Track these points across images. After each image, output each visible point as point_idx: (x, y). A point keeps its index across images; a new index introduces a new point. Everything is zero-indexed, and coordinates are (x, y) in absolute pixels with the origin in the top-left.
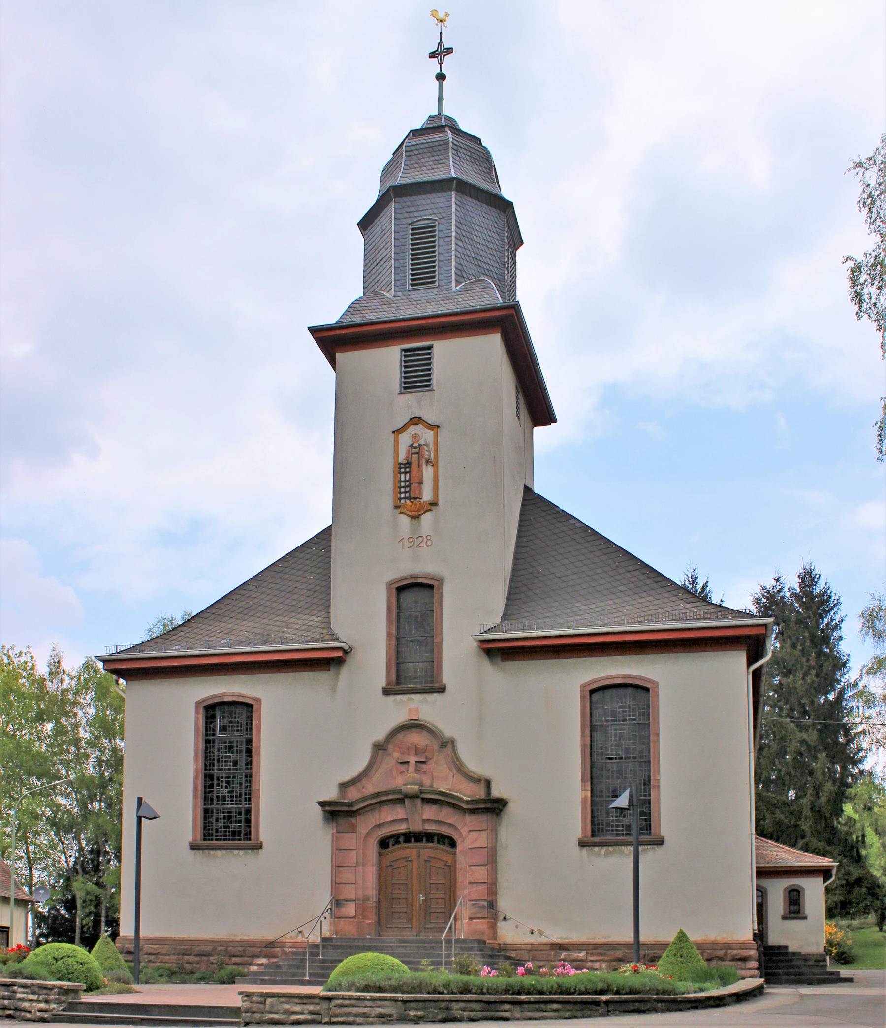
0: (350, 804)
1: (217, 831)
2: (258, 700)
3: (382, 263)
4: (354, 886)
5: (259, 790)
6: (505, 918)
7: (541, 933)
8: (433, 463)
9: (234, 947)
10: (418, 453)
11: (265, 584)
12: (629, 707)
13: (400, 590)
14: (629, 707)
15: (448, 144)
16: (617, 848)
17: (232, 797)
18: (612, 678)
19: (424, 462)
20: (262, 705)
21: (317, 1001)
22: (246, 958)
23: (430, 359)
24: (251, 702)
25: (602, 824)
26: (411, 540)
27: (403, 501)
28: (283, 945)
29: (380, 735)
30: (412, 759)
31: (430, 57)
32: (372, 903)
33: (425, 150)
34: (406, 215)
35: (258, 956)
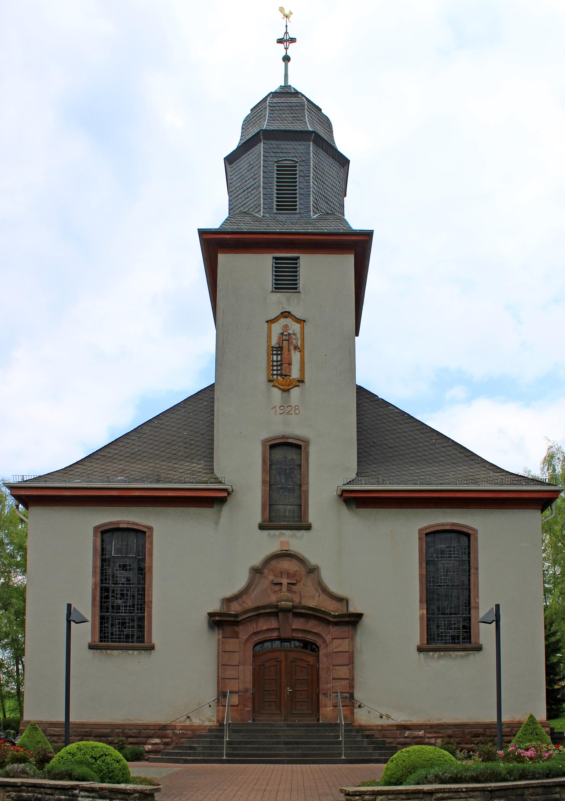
0: (236, 616)
1: (112, 634)
2: (151, 529)
3: (250, 190)
4: (237, 681)
5: (151, 602)
6: (360, 706)
7: (388, 717)
8: (300, 349)
9: (130, 730)
10: (288, 340)
11: (145, 436)
12: (454, 547)
13: (272, 447)
14: (454, 547)
15: (303, 106)
17: (126, 606)
18: (443, 525)
19: (292, 347)
20: (154, 533)
21: (421, 796)
22: (141, 739)
23: (296, 268)
24: (145, 530)
25: (434, 635)
26: (282, 408)
27: (275, 377)
28: (174, 728)
29: (257, 560)
30: (285, 581)
31: (278, 42)
32: (249, 694)
33: (286, 108)
34: (273, 155)
35: (151, 737)
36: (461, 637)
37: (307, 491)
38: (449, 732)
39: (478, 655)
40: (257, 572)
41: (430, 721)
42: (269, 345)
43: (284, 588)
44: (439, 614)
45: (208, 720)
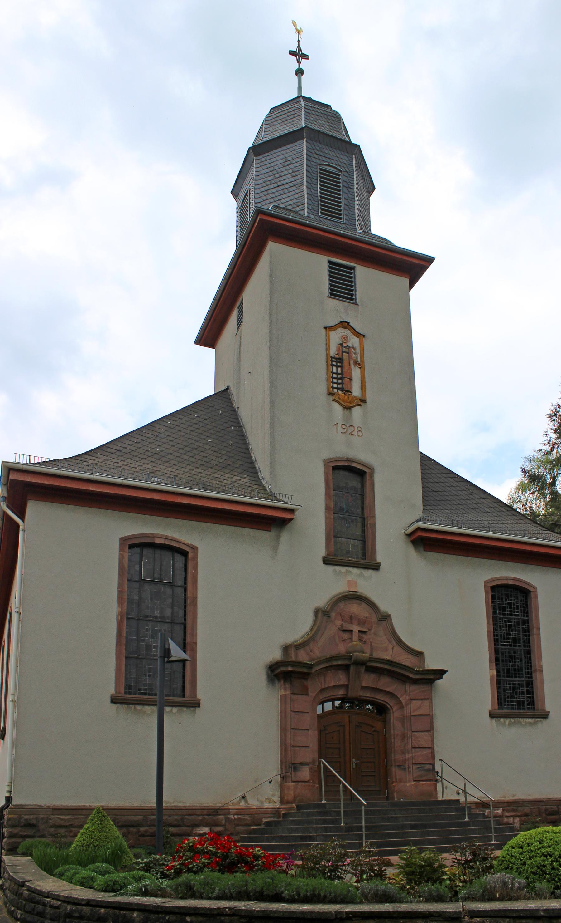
2: (195, 549)
3: (287, 186)
8: (360, 365)
9: (170, 816)
10: (348, 353)
13: (335, 468)
16: (517, 720)
18: (507, 579)
19: (352, 362)
20: (199, 554)
22: (184, 828)
24: (187, 549)
26: (344, 426)
28: (226, 812)
29: (322, 600)
30: (356, 628)
31: (290, 54)
35: (198, 826)
36: (526, 703)
37: (374, 525)
38: (526, 809)
39: (545, 722)
40: (322, 614)
41: (505, 797)
43: (355, 636)
44: (504, 677)
45: (267, 801)
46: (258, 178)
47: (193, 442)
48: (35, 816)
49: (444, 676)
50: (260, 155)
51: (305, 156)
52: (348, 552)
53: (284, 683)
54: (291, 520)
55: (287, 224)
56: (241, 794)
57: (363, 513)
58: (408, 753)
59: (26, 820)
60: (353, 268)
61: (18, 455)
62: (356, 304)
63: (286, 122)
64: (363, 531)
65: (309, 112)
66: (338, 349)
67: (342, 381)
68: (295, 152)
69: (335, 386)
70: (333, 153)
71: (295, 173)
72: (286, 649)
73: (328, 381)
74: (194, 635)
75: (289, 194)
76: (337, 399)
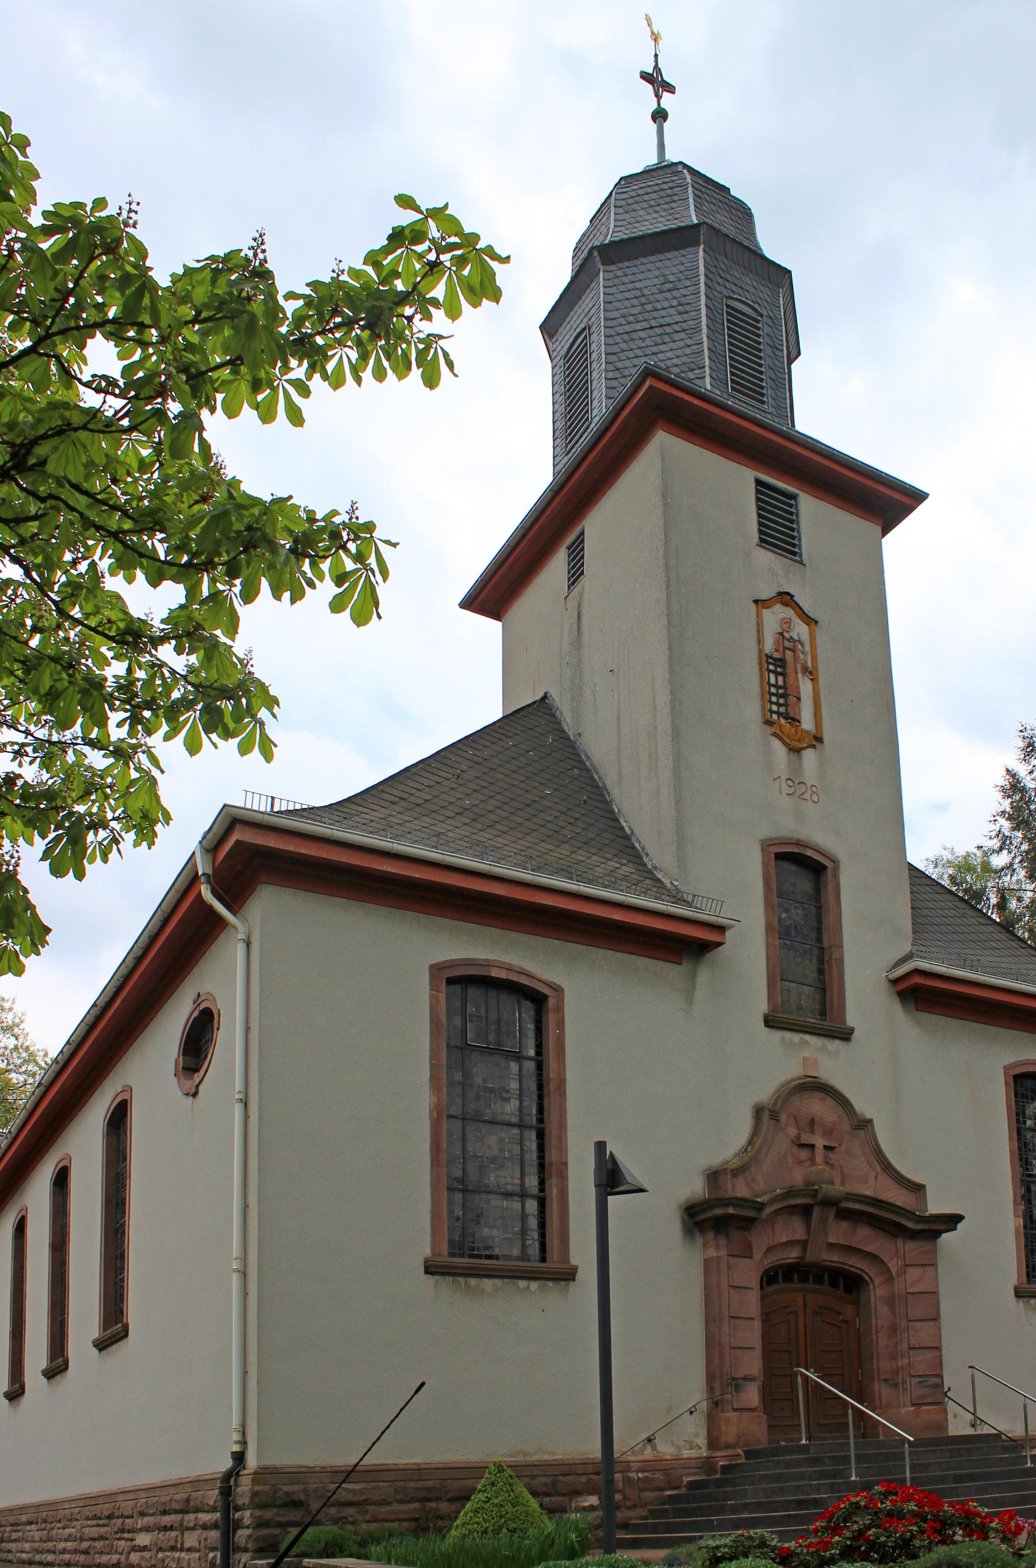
3: (668, 329)
8: (811, 673)
10: (793, 651)
13: (779, 856)
19: (799, 667)
24: (546, 991)
26: (790, 783)
29: (764, 1092)
31: (642, 77)
35: (578, 1493)
42: (760, 651)
43: (819, 1157)
46: (609, 307)
47: (521, 792)
48: (302, 1487)
49: (959, 1226)
50: (614, 264)
51: (702, 278)
52: (800, 1008)
53: (715, 1237)
54: (719, 944)
55: (696, 402)
56: (645, 1435)
57: (819, 939)
58: (902, 1356)
59: (286, 1493)
60: (793, 497)
61: (250, 795)
62: (801, 563)
63: (657, 208)
64: (821, 971)
65: (700, 195)
66: (777, 643)
67: (786, 701)
68: (682, 268)
69: (774, 708)
70: (748, 280)
71: (686, 307)
72: (714, 1176)
73: (762, 698)
74: (563, 1149)
75: (672, 346)
76: (778, 732)
